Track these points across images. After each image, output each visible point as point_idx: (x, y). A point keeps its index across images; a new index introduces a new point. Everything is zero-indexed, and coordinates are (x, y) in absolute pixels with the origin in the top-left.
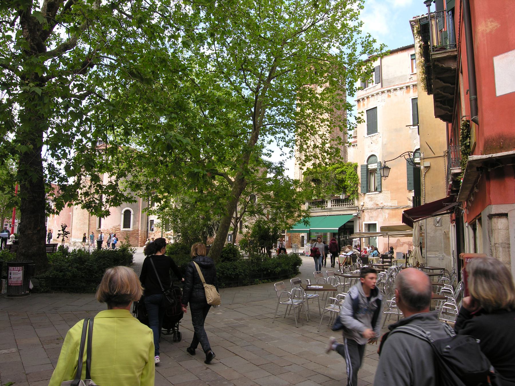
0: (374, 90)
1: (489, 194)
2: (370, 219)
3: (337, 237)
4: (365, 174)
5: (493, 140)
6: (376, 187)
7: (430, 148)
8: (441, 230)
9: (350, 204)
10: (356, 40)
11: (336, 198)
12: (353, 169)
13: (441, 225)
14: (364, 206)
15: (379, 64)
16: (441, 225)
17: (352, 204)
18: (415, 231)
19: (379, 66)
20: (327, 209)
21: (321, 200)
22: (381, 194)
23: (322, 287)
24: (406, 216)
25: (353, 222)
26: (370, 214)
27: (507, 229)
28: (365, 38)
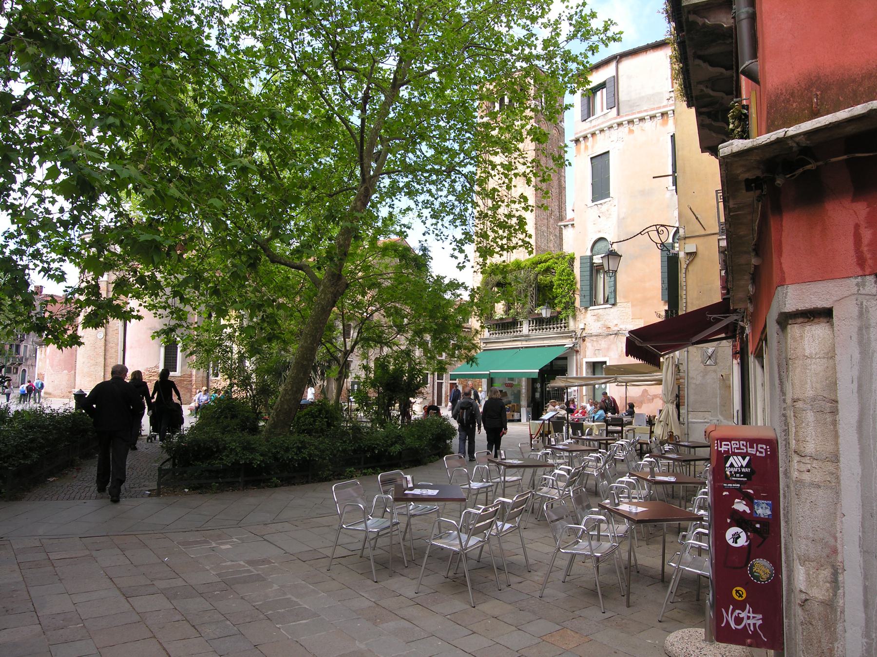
0: (604, 120)
1: (780, 254)
2: (595, 354)
3: (538, 385)
4: (588, 273)
5: (792, 94)
6: (606, 296)
7: (697, 218)
8: (715, 371)
9: (561, 327)
10: (560, 14)
11: (536, 317)
12: (566, 264)
13: (716, 363)
14: (586, 331)
15: (614, 74)
16: (716, 363)
17: (565, 327)
18: (666, 373)
19: (614, 77)
20: (522, 336)
21: (511, 320)
22: (615, 309)
23: (434, 492)
24: (638, 342)
25: (566, 358)
26: (595, 344)
27: (831, 355)
28: (575, 8)
